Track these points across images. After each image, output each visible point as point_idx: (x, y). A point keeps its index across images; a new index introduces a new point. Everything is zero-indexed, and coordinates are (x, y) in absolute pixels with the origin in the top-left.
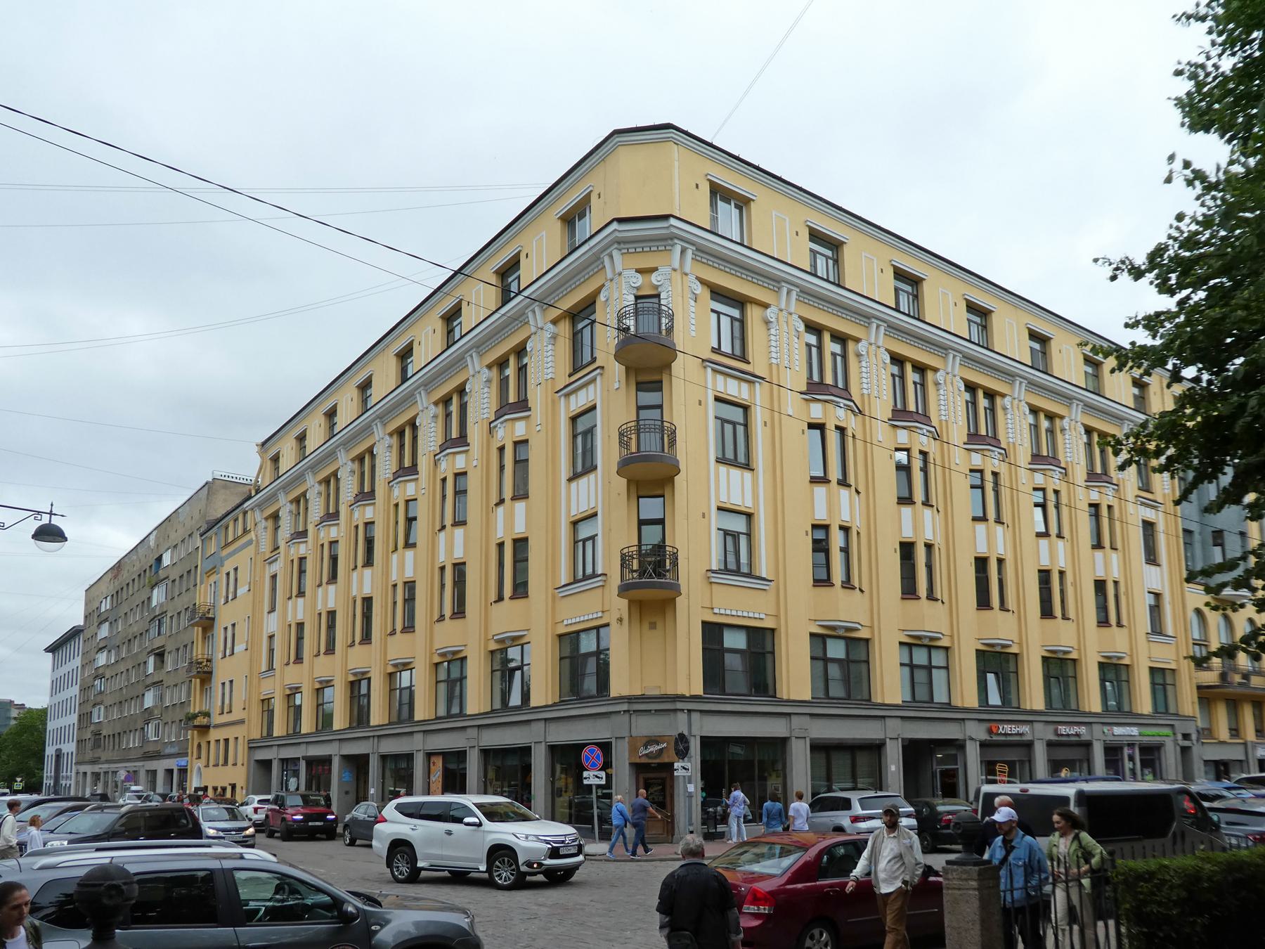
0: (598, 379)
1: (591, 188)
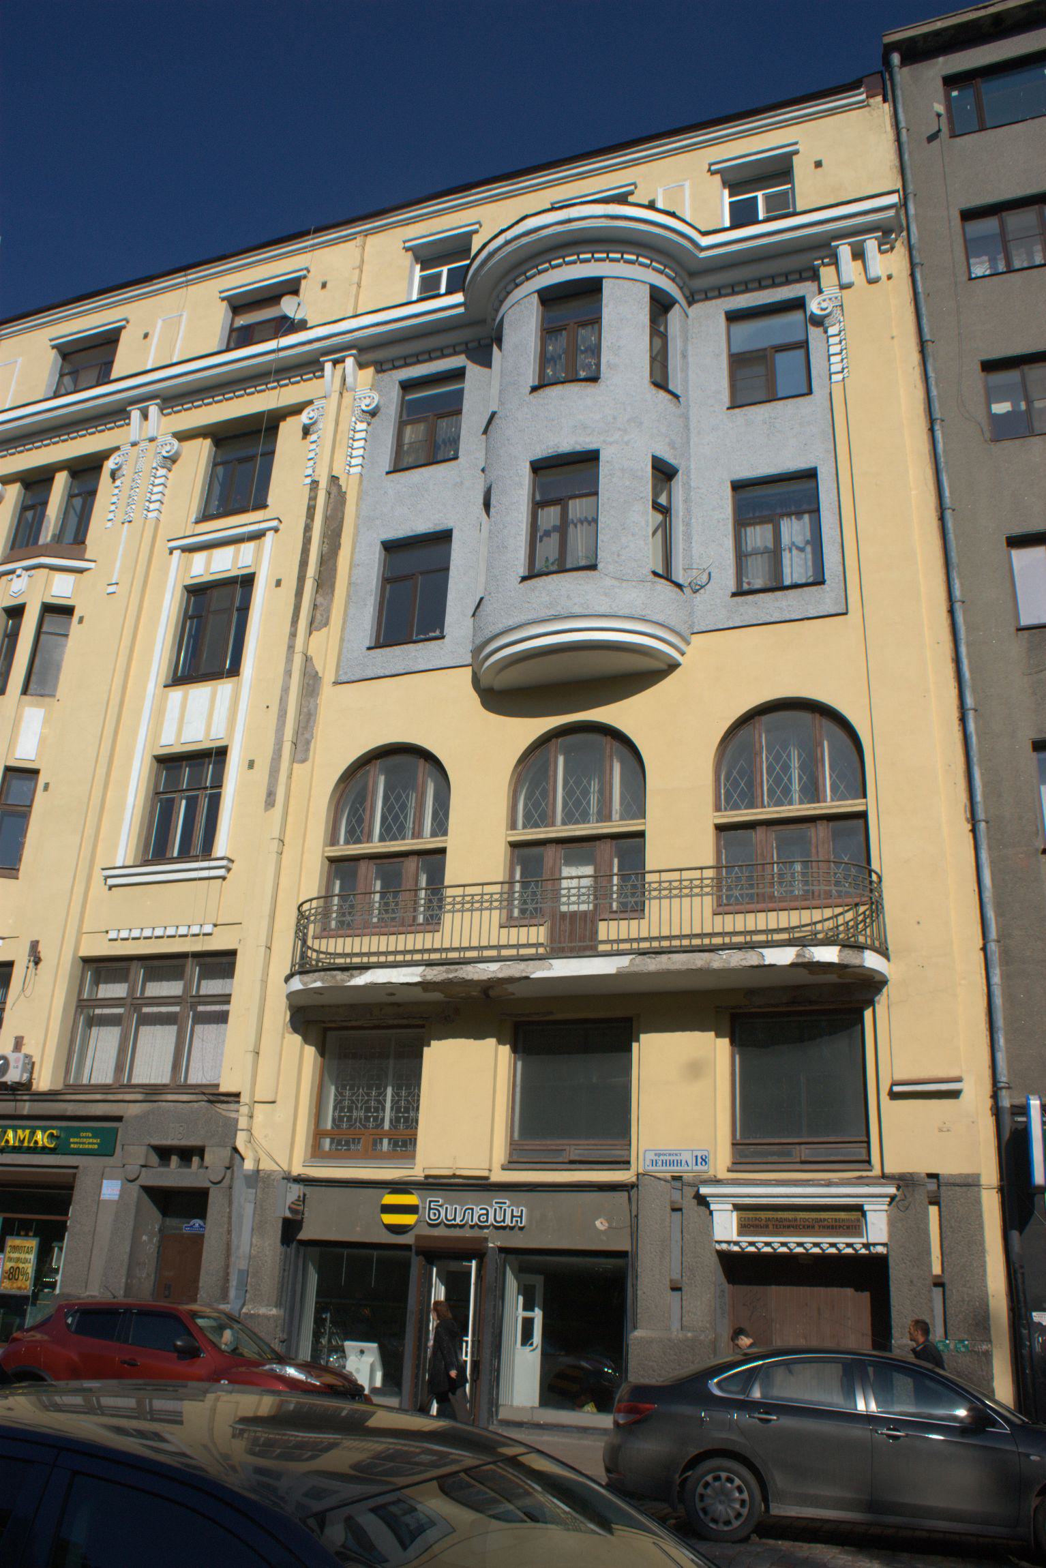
0: (270, 534)
1: (123, 323)
